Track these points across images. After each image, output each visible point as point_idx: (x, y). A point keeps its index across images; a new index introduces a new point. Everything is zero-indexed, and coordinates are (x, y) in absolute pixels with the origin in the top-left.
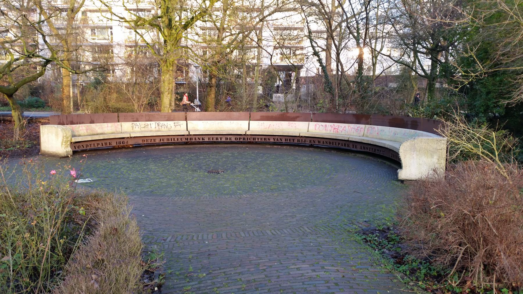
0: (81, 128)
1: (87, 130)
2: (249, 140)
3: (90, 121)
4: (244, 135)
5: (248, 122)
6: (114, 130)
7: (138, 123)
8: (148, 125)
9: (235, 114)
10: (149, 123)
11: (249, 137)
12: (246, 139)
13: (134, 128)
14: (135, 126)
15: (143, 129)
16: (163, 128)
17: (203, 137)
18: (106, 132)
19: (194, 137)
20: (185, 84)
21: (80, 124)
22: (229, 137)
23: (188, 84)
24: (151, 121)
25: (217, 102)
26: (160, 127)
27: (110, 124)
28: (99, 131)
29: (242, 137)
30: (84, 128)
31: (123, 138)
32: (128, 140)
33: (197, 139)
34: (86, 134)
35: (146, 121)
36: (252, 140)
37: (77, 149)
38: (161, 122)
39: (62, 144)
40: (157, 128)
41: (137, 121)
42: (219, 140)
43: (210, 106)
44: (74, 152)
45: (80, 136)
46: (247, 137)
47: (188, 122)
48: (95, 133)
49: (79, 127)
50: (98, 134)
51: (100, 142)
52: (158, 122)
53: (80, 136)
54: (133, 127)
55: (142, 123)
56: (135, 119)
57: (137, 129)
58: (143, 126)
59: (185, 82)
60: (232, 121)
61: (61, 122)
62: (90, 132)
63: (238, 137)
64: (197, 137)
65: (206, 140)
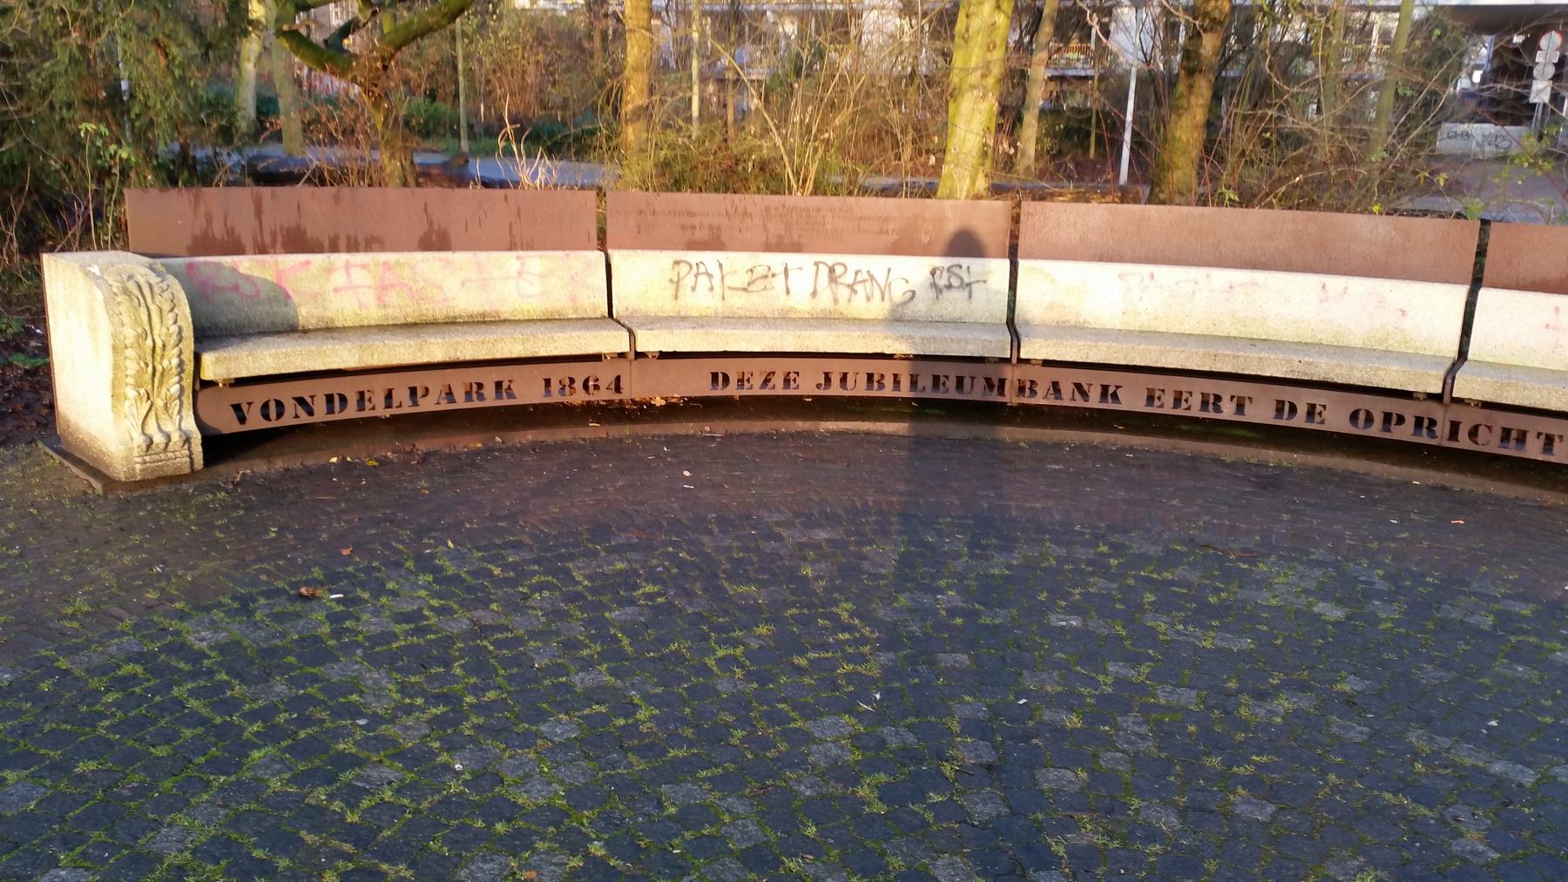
0: (339, 279)
1: (382, 289)
2: (1464, 442)
3: (419, 230)
4: (1437, 398)
5: (1462, 292)
6: (557, 299)
7: (709, 258)
8: (769, 275)
9: (1370, 228)
10: (776, 260)
11: (1467, 420)
12: (1442, 430)
13: (685, 291)
14: (689, 281)
15: (738, 302)
16: (859, 299)
17: (1111, 378)
18: (506, 311)
19: (1044, 378)
20: (1092, 78)
21: (353, 247)
22: (1303, 398)
23: (1102, 78)
24: (797, 248)
25: (1212, 148)
26: (843, 293)
27: (536, 261)
28: (466, 302)
29: (1410, 410)
30: (359, 276)
31: (596, 358)
32: (622, 368)
33: (1067, 388)
34: (374, 315)
35: (769, 247)
36: (1490, 443)
37: (227, 424)
38: (855, 262)
39: (117, 397)
40: (824, 301)
41: (714, 243)
42: (1228, 412)
43: (1180, 161)
44: (218, 447)
45: (291, 330)
46: (1456, 413)
47: (1023, 264)
48: (437, 311)
49: (329, 270)
50: (451, 323)
51: (434, 381)
52: (831, 259)
53: (329, 330)
54: (677, 283)
55: (737, 263)
56: (701, 235)
57: (700, 300)
58: (741, 279)
59: (1090, 73)
60: (1335, 282)
61: (218, 230)
62: (400, 307)
63: (1379, 406)
64: (1067, 379)
65: (1132, 400)
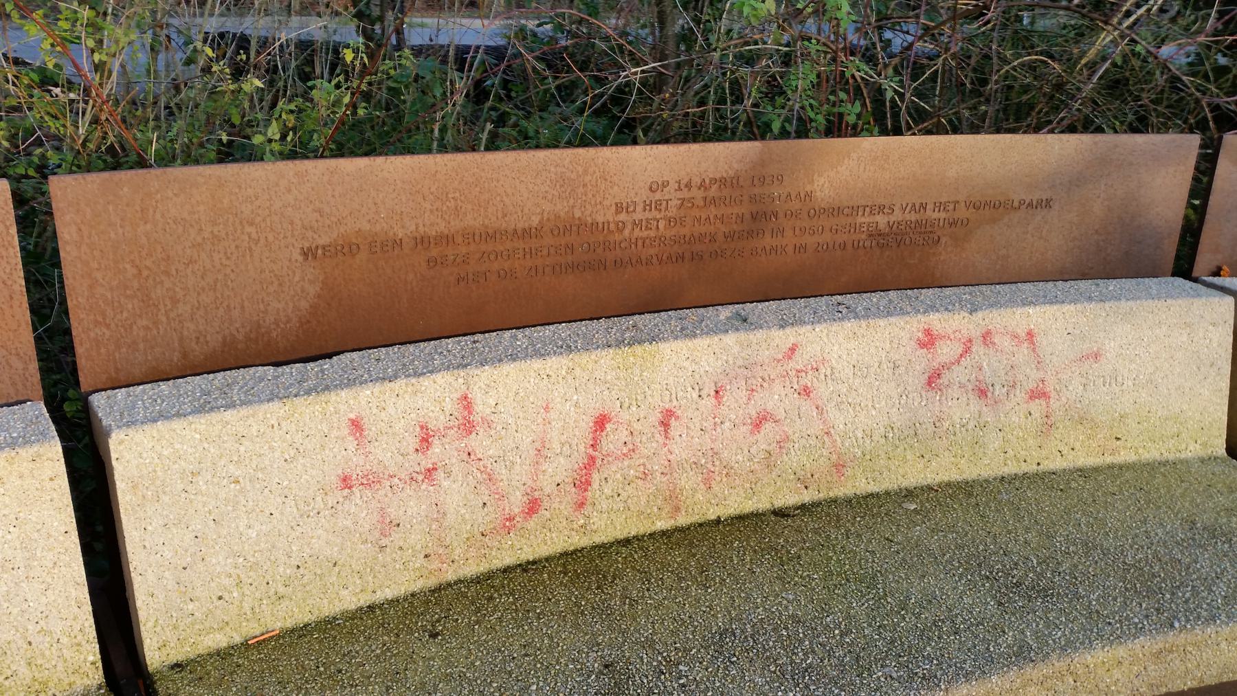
47: (145, 452)
